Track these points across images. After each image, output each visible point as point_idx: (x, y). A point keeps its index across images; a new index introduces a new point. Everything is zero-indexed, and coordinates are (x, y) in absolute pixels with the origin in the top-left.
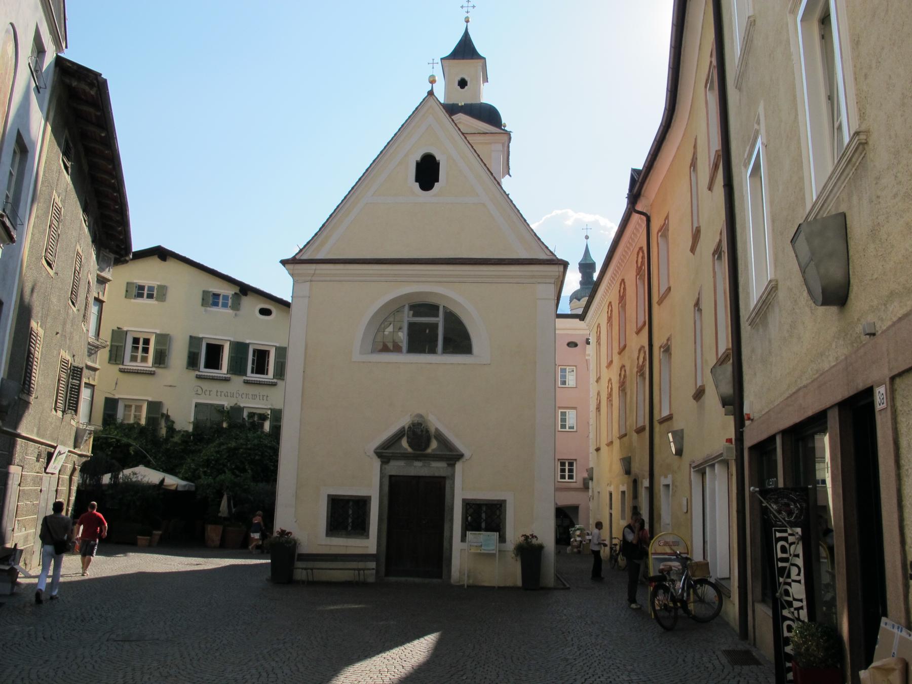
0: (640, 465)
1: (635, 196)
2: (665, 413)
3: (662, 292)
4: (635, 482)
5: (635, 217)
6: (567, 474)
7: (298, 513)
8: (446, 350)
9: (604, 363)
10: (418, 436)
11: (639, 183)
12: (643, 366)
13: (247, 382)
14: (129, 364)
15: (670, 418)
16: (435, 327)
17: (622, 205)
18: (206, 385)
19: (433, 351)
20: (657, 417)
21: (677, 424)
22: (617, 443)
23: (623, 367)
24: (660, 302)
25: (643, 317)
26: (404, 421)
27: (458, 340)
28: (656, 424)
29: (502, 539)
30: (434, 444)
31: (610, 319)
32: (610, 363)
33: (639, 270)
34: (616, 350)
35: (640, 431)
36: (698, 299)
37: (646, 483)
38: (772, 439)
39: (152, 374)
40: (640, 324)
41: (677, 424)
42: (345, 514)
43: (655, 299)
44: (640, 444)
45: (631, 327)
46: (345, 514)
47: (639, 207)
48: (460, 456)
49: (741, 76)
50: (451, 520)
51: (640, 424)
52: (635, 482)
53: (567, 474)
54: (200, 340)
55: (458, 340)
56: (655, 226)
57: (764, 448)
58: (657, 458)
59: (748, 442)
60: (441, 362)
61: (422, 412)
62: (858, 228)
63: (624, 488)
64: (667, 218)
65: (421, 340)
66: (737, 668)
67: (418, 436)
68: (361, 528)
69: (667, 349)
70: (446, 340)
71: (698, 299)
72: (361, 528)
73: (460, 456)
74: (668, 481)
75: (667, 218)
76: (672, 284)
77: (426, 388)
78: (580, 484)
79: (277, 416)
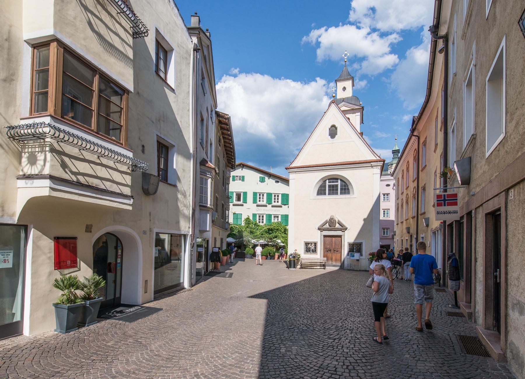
0: (413, 230)
1: (413, 130)
2: (423, 211)
3: (423, 166)
4: (411, 236)
5: (413, 138)
6: (261, 221)
7: (295, 246)
8: (341, 193)
9: (400, 193)
10: (332, 222)
11: (415, 122)
12: (415, 194)
13: (273, 206)
14: (259, 203)
15: (424, 213)
16: (337, 186)
17: (408, 133)
18: (259, 208)
19: (337, 194)
20: (420, 213)
21: (427, 216)
22: (405, 222)
23: (407, 194)
24: (422, 171)
25: (415, 176)
26: (328, 218)
27: (346, 188)
28: (419, 215)
29: (361, 255)
30: (337, 226)
31: (403, 176)
32: (402, 193)
33: (414, 158)
34: (405, 188)
35: (414, 217)
36: (249, 297)
37: (415, 236)
38: (453, 222)
39: (242, 205)
40: (414, 178)
41: (427, 216)
42: (310, 248)
43: (420, 169)
44: (412, 223)
45: (411, 179)
46: (310, 248)
47: (415, 134)
48: (346, 229)
49: (454, 83)
50: (344, 249)
51: (414, 215)
52: (411, 236)
53: (261, 221)
54: (256, 193)
55: (346, 188)
56: (421, 141)
57: (451, 225)
58: (419, 228)
59: (447, 224)
60: (339, 198)
61: (333, 215)
62: (472, 157)
63: (407, 238)
64: (426, 138)
65: (333, 190)
66: (438, 293)
67: (332, 222)
68: (315, 251)
69: (424, 189)
70: (341, 189)
71: (249, 297)
72: (315, 251)
73: (346, 229)
74: (423, 236)
75: (426, 138)
76: (427, 164)
77: (335, 206)
78: (391, 237)
79: (286, 217)
